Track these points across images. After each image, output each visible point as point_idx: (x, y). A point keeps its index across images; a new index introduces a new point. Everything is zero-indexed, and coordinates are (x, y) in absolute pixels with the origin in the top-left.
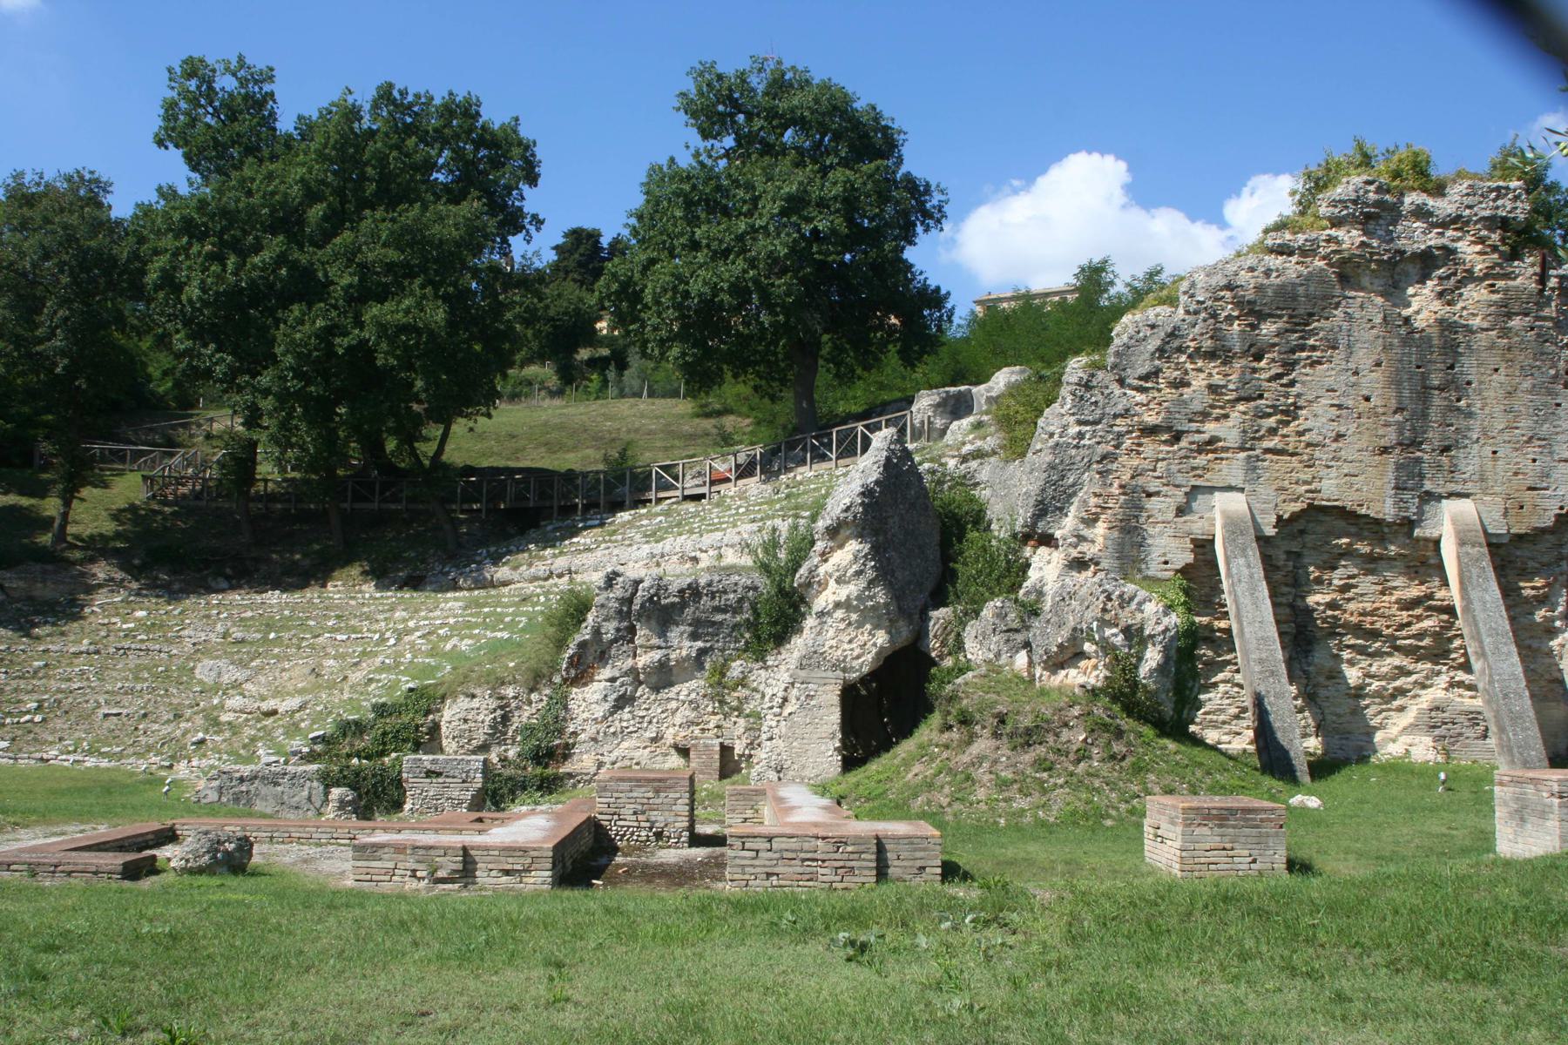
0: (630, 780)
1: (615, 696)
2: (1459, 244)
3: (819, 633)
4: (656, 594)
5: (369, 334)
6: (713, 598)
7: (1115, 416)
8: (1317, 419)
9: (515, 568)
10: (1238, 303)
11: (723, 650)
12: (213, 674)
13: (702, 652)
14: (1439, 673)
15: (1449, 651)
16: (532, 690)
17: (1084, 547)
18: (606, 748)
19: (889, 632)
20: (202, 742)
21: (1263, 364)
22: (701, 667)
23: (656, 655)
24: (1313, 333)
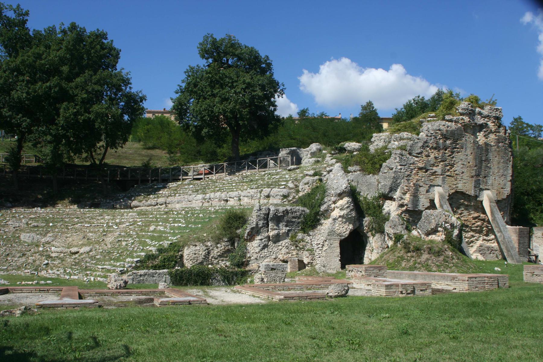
0: (373, 267)
1: (263, 245)
2: (488, 123)
5: (92, 116)
7: (411, 164)
8: (458, 168)
9: (140, 201)
10: (442, 135)
11: (294, 230)
12: (31, 239)
13: (289, 231)
14: (480, 237)
15: (483, 231)
16: (218, 243)
17: (403, 201)
18: (260, 262)
20: (47, 264)
21: (447, 152)
23: (276, 232)
24: (458, 144)
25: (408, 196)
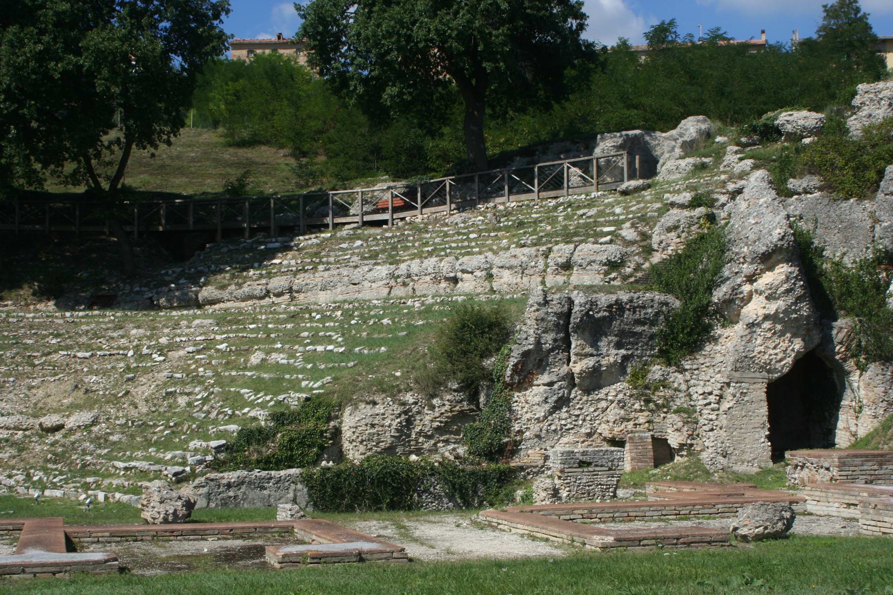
0: (861, 456)
1: (555, 398)
3: (749, 341)
4: (590, 310)
5: (85, 62)
6: (634, 312)
9: (223, 287)
11: (640, 357)
13: (626, 358)
16: (433, 396)
18: (548, 445)
19: (803, 340)
22: (623, 371)
23: (590, 362)
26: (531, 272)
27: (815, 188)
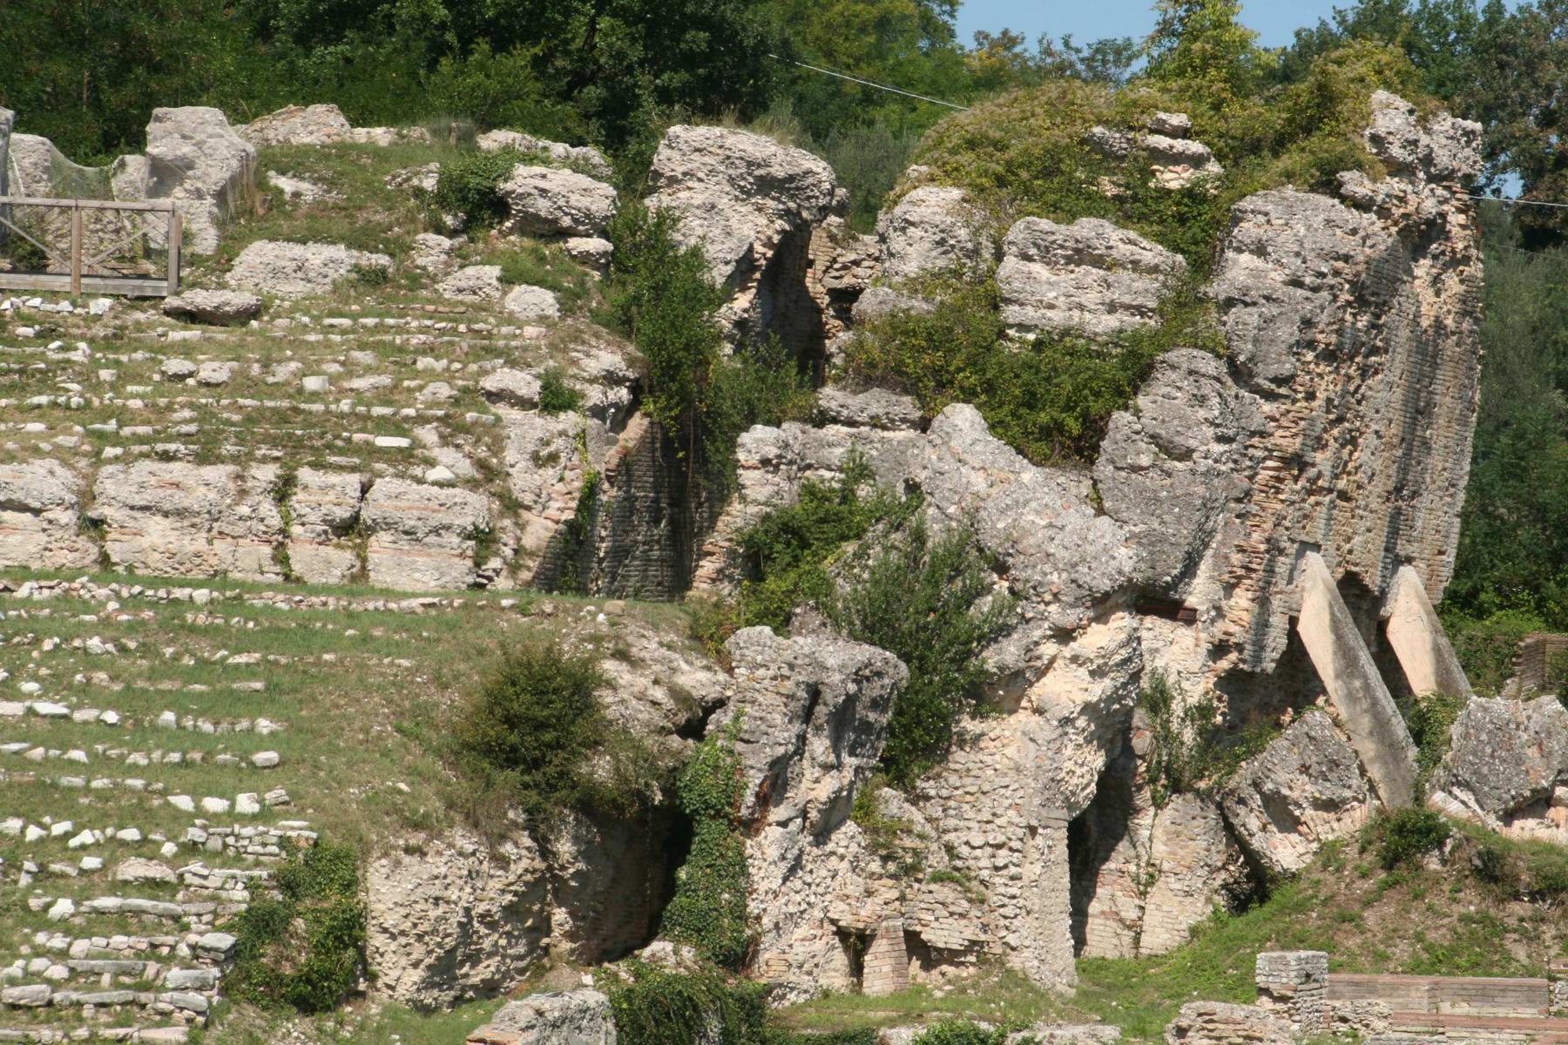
25: (1242, 600)
26: (240, 528)
27: (903, 421)
